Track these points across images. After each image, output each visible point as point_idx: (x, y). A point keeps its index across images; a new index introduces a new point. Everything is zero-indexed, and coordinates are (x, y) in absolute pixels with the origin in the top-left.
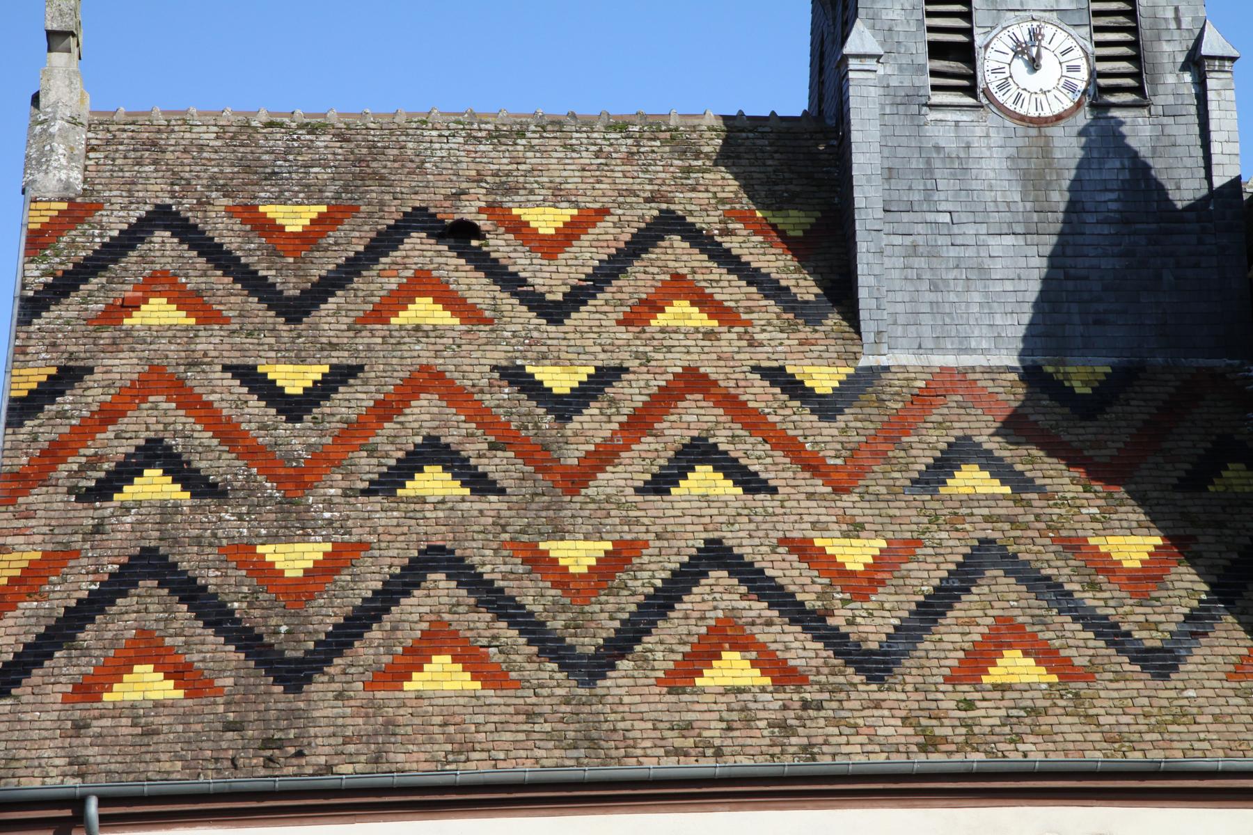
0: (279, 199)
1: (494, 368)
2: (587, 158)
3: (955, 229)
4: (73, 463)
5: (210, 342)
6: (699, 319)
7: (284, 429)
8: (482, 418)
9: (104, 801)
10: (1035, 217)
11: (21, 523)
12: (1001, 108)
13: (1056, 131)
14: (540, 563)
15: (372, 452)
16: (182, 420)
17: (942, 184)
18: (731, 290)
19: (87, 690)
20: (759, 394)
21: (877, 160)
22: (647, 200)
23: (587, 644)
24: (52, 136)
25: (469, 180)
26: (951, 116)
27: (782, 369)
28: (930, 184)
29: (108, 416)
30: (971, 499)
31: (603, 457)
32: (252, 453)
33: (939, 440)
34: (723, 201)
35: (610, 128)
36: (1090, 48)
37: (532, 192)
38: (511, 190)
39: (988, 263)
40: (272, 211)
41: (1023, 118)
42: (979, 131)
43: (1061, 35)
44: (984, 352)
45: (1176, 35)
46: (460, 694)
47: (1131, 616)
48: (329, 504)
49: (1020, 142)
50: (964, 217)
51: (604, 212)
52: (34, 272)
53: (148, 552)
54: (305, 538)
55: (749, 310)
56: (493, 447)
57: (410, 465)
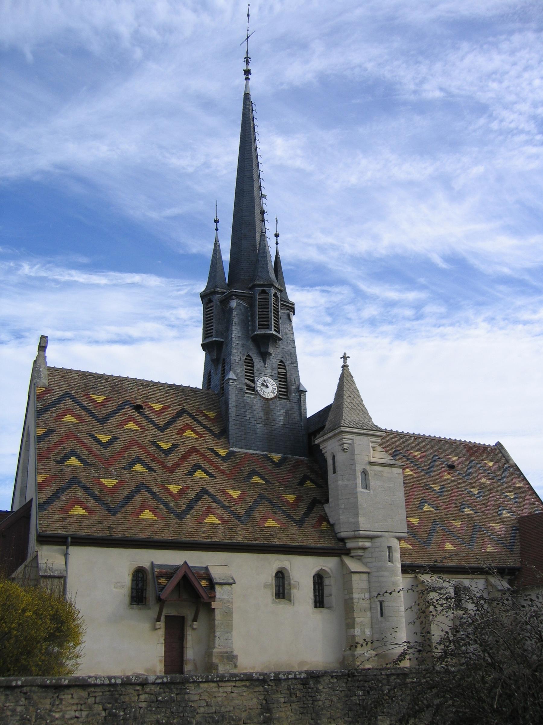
1: (150, 441)
2: (164, 393)
3: (250, 421)
4: (54, 454)
5: (82, 427)
6: (193, 435)
7: (102, 451)
8: (147, 452)
9: (72, 538)
10: (266, 421)
11: (43, 467)
12: (260, 395)
13: (271, 402)
14: (167, 490)
15: (124, 458)
17: (248, 411)
18: (200, 430)
19: (65, 510)
20: (209, 454)
21: (234, 403)
22: (179, 405)
23: (179, 510)
24: (40, 371)
25: (138, 395)
26: (250, 396)
27: (213, 449)
28: (245, 410)
29: (60, 443)
30: (257, 484)
31: (177, 465)
32: (96, 456)
33: (172, 456)
36: (278, 385)
37: (153, 400)
39: (256, 430)
41: (264, 398)
42: (255, 400)
43: (272, 381)
44: (254, 450)
45: (295, 385)
46: (152, 519)
47: (292, 512)
48: (116, 471)
49: (264, 403)
50: (252, 419)
51: (169, 407)
52: (39, 404)
54: (111, 478)
56: (152, 460)
57: (133, 463)
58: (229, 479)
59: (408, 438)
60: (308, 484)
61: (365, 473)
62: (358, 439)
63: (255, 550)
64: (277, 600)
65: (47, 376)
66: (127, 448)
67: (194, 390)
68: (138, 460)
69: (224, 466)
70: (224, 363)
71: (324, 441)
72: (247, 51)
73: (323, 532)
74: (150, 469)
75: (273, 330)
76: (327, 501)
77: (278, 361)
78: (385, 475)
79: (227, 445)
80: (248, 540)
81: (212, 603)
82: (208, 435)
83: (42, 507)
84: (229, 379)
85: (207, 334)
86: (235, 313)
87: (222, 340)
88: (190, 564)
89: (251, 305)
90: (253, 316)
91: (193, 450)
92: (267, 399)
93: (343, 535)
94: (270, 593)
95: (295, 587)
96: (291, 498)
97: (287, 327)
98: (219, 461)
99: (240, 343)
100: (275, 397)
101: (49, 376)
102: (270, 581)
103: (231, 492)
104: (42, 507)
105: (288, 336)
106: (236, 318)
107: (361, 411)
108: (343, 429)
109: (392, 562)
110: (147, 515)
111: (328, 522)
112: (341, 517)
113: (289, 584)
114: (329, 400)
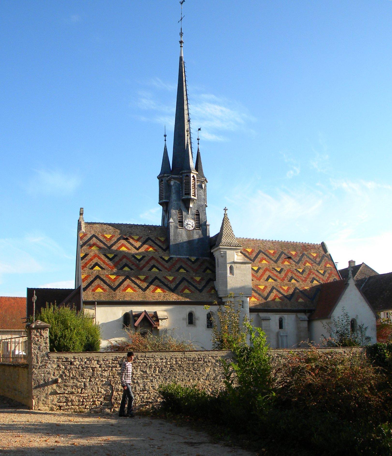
0: (106, 234)
16: (99, 260)
19: (94, 290)
20: (160, 260)
22: (147, 236)
23: (144, 288)
26: (180, 229)
29: (91, 260)
30: (182, 273)
31: (144, 266)
33: (169, 263)
34: (155, 236)
35: (142, 226)
38: (132, 234)
40: (106, 235)
41: (188, 230)
46: (131, 292)
47: (198, 286)
51: (142, 237)
53: (98, 276)
55: (158, 250)
57: (124, 267)
58: (169, 271)
59: (269, 243)
60: (208, 271)
61: (231, 268)
62: (228, 252)
63: (22, 346)
64: (189, 325)
65: (84, 227)
66: (121, 260)
67: (155, 227)
68: (126, 265)
69: (167, 265)
70: (169, 213)
71: (214, 251)
72: (181, 28)
73: (212, 294)
74: (131, 269)
75: (191, 196)
76: (215, 280)
77: (196, 210)
78: (242, 267)
79: (169, 254)
80: (175, 299)
81: (158, 327)
82: (160, 250)
83: (85, 289)
84: (170, 222)
85: (161, 198)
86: (173, 187)
87: (168, 201)
88: (146, 311)
89: (182, 183)
90: (182, 188)
91: (153, 258)
92: (190, 231)
93: (220, 296)
94: (186, 322)
95: (197, 319)
96: (198, 279)
97: (200, 192)
98: (164, 263)
99: (176, 203)
100: (194, 229)
101: (85, 227)
102: (186, 317)
103: (168, 278)
104: (85, 289)
105: (201, 197)
106: (173, 190)
107: (232, 237)
108: (221, 247)
109: (244, 308)
110: (129, 290)
111: (215, 289)
112: (220, 288)
113: (195, 318)
114: (218, 231)
